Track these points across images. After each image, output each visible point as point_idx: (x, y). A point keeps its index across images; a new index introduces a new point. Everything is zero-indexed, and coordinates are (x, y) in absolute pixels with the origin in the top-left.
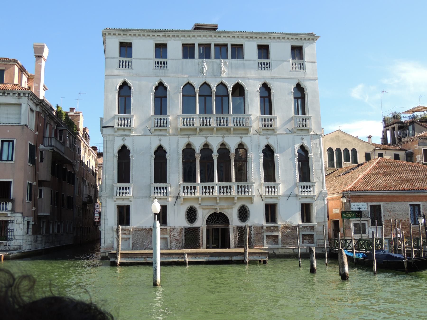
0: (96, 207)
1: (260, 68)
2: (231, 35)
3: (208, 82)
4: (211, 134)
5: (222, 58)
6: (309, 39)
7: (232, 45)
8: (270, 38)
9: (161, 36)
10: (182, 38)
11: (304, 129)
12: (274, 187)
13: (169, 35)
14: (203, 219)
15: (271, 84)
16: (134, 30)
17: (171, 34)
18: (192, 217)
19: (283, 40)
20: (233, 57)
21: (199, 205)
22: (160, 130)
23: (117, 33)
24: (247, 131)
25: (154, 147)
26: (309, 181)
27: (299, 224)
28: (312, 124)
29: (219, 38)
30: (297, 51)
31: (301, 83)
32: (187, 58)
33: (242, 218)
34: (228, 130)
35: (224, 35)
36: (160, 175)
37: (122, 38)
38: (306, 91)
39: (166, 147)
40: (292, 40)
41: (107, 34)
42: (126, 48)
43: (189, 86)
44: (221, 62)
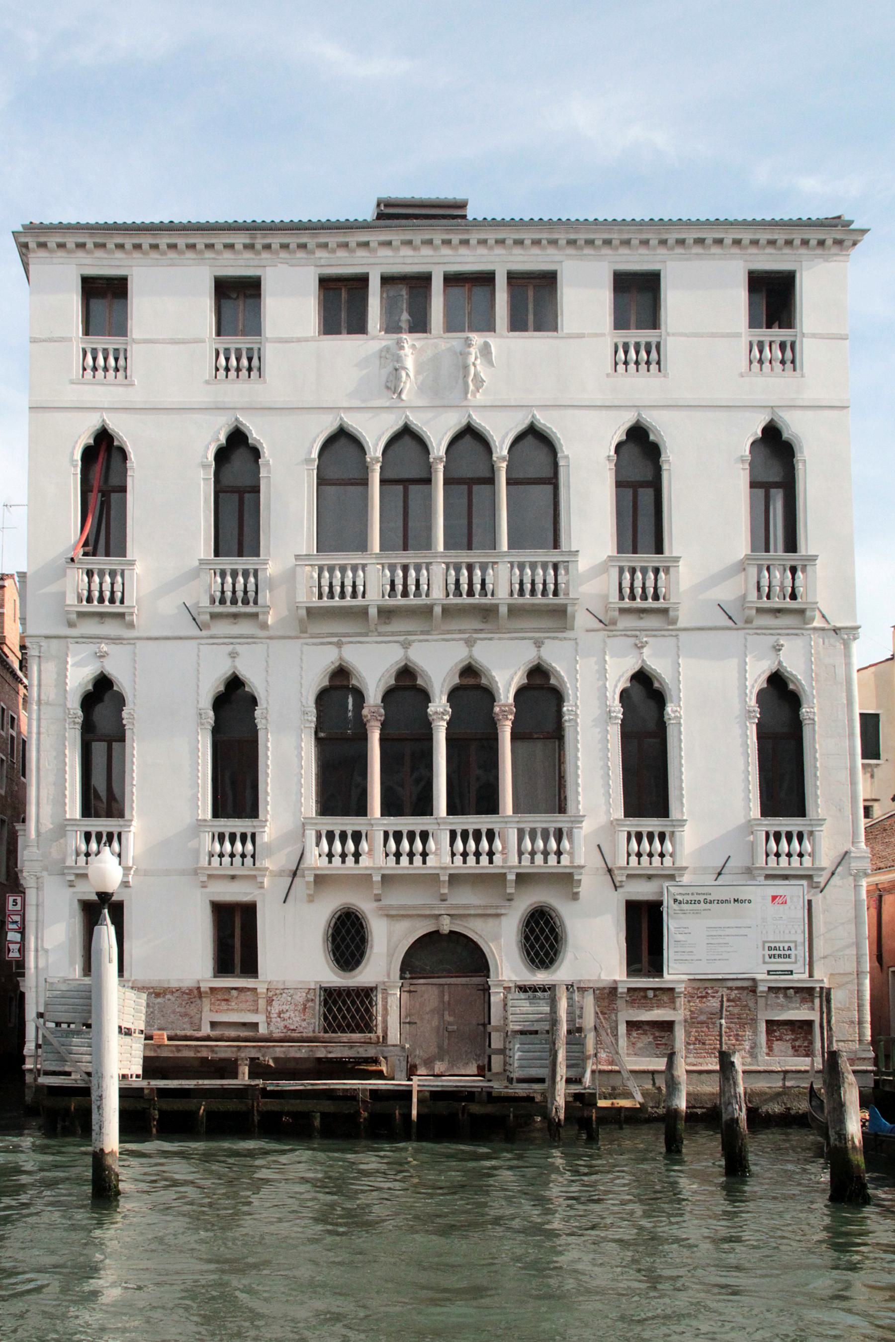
0: (11, 907)
1: (621, 367)
2: (511, 236)
3: (418, 421)
4: (423, 633)
5: (472, 329)
6: (821, 243)
7: (512, 277)
8: (663, 242)
9: (239, 247)
10: (320, 254)
11: (787, 610)
12: (662, 837)
13: (267, 241)
14: (391, 955)
15: (795, 426)
16: (512, 224)
17: (275, 240)
18: (348, 947)
19: (715, 250)
20: (517, 324)
21: (376, 904)
22: (235, 616)
23: (71, 241)
24: (558, 615)
25: (211, 684)
26: (801, 812)
27: (615, 982)
28: (820, 589)
29: (463, 251)
30: (774, 299)
31: (780, 424)
32: (339, 332)
33: (537, 954)
34: (488, 613)
35: (483, 236)
36: (236, 786)
37: (88, 261)
38: (799, 456)
39: (255, 681)
40: (753, 250)
41: (32, 245)
42: (104, 296)
43: (342, 440)
44: (468, 343)
